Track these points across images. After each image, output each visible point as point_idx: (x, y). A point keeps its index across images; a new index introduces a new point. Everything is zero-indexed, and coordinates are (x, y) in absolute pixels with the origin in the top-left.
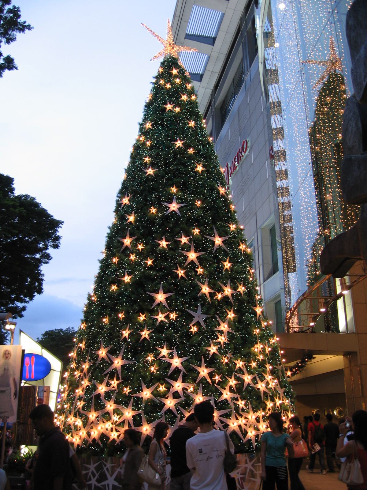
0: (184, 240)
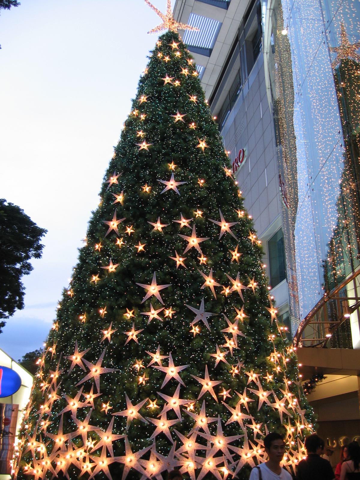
0: (184, 222)
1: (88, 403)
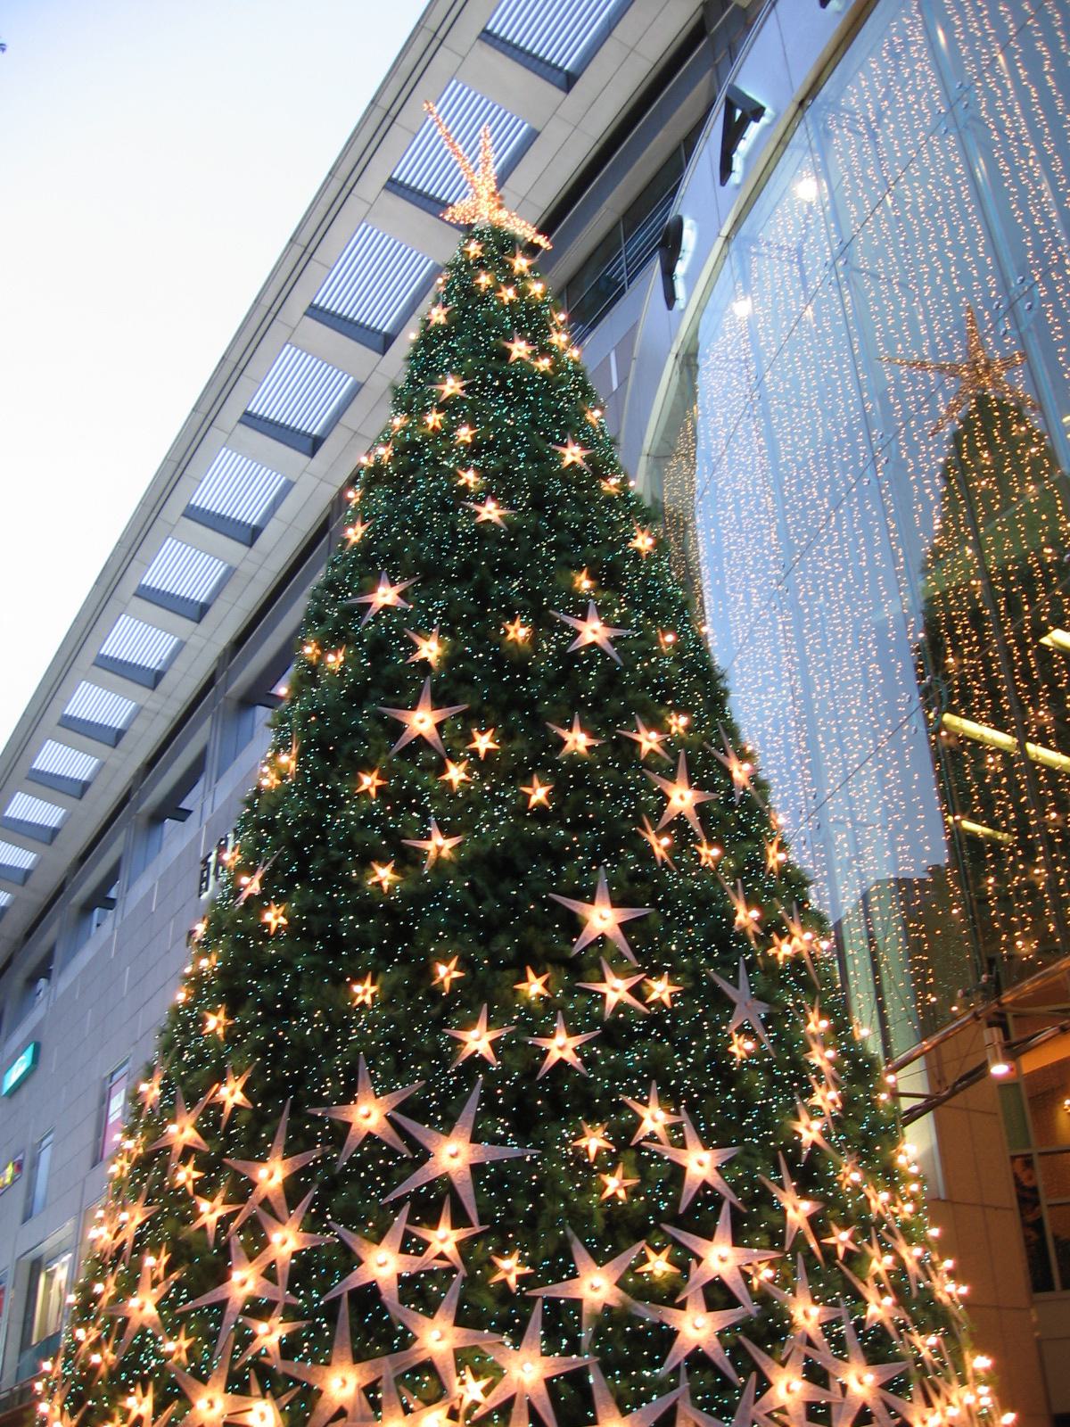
1: (436, 1258)
